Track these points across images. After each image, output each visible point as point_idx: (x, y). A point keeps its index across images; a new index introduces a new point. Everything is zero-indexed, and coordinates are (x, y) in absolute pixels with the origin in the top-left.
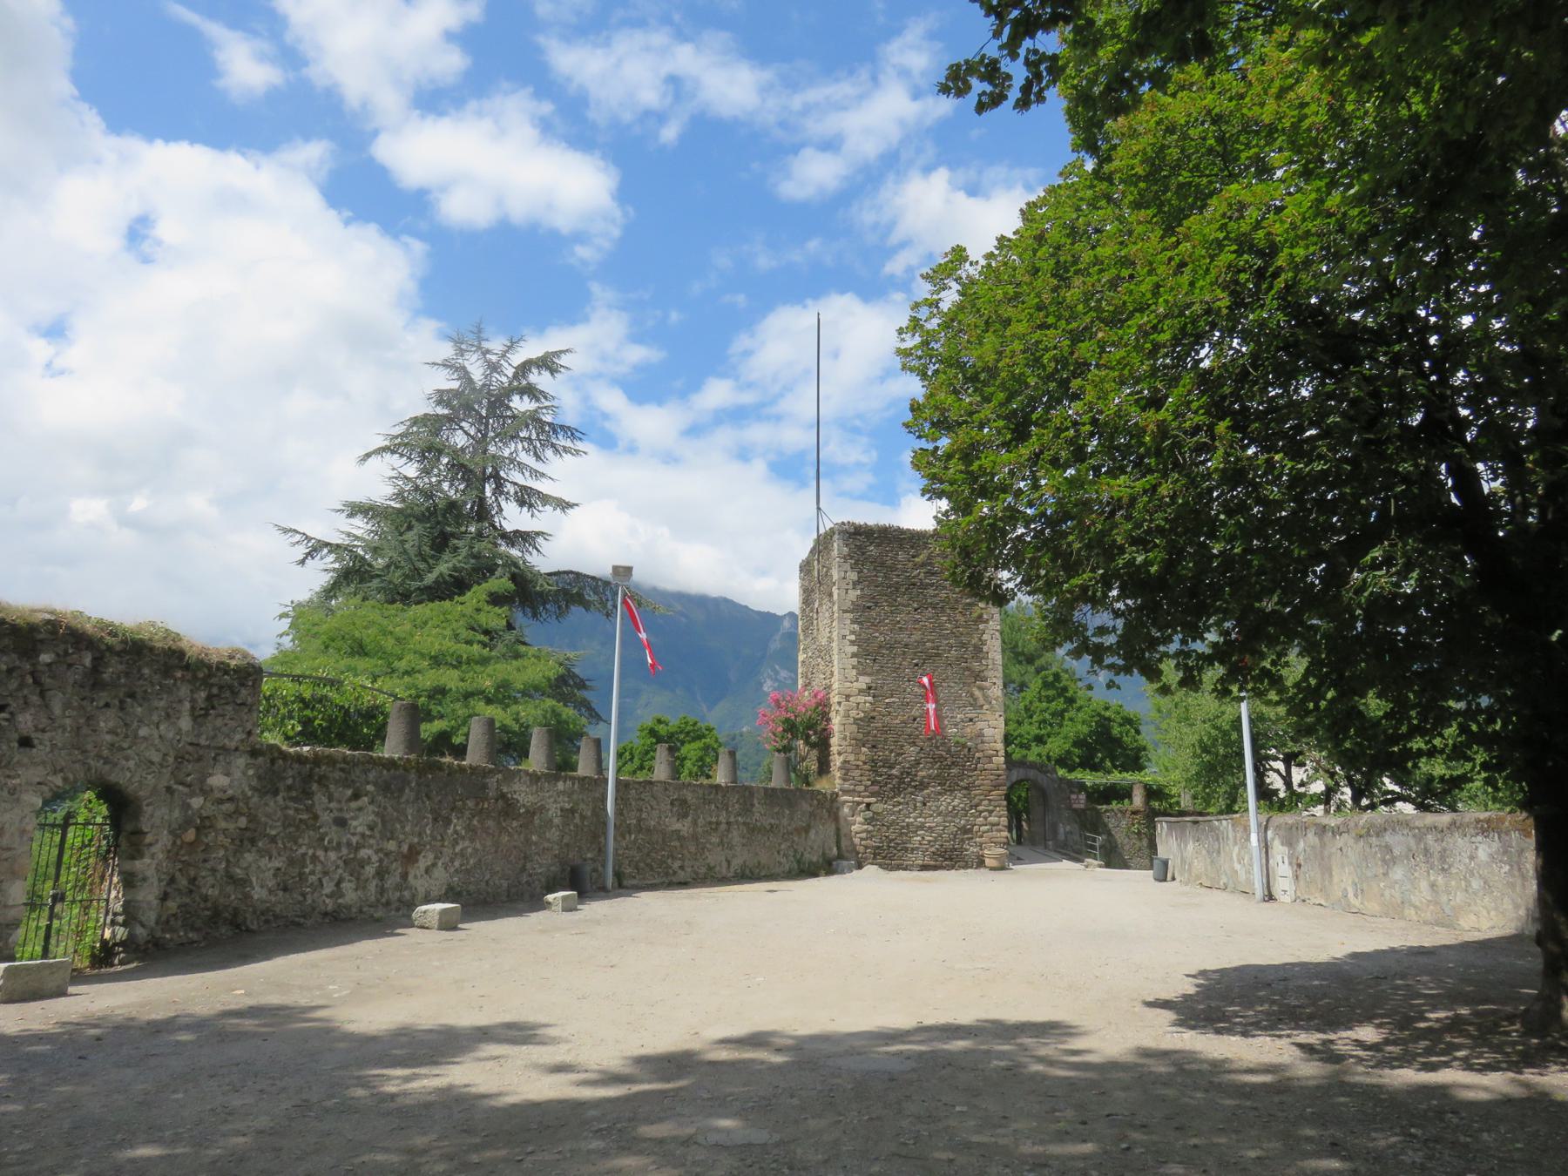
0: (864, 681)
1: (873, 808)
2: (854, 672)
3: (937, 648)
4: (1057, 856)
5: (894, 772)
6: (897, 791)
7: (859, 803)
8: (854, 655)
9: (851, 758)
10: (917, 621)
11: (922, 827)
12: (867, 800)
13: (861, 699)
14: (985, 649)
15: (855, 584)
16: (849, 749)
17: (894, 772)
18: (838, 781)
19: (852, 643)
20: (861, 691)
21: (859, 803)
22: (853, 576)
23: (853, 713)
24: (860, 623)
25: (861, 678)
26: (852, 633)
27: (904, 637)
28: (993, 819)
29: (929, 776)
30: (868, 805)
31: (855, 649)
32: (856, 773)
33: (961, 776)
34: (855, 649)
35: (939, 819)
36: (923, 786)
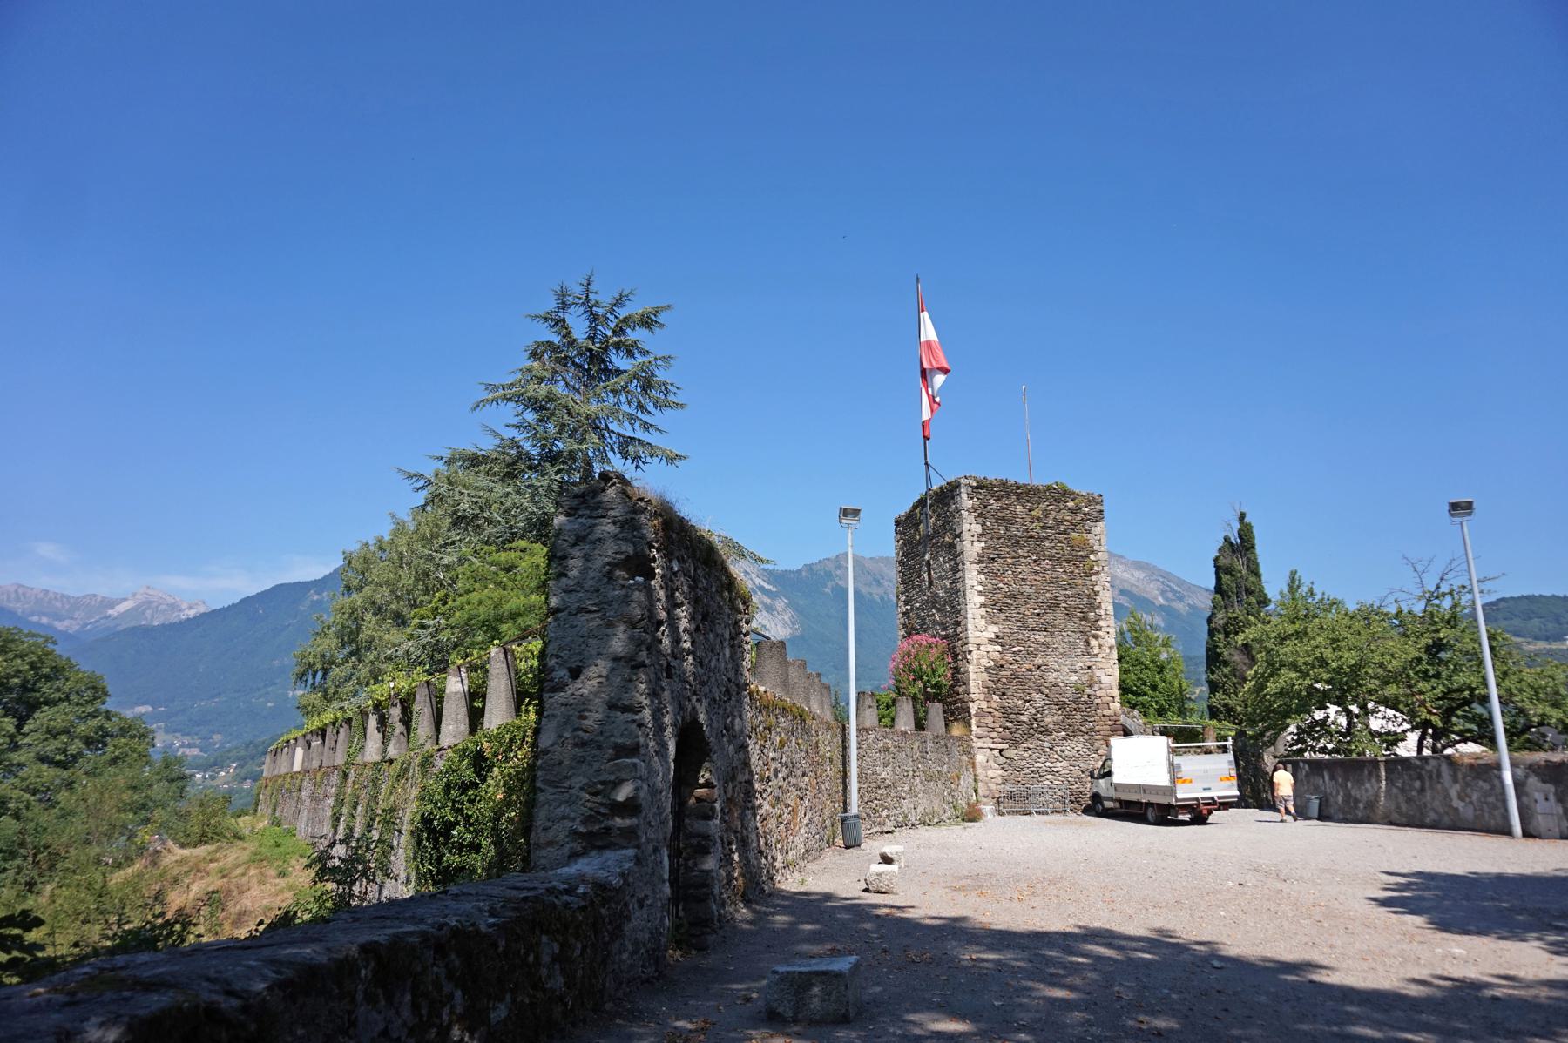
1: (1005, 753)
5: (1021, 718)
8: (983, 605)
9: (984, 705)
13: (991, 648)
17: (1021, 718)
23: (984, 662)
32: (989, 720)
35: (1065, 763)
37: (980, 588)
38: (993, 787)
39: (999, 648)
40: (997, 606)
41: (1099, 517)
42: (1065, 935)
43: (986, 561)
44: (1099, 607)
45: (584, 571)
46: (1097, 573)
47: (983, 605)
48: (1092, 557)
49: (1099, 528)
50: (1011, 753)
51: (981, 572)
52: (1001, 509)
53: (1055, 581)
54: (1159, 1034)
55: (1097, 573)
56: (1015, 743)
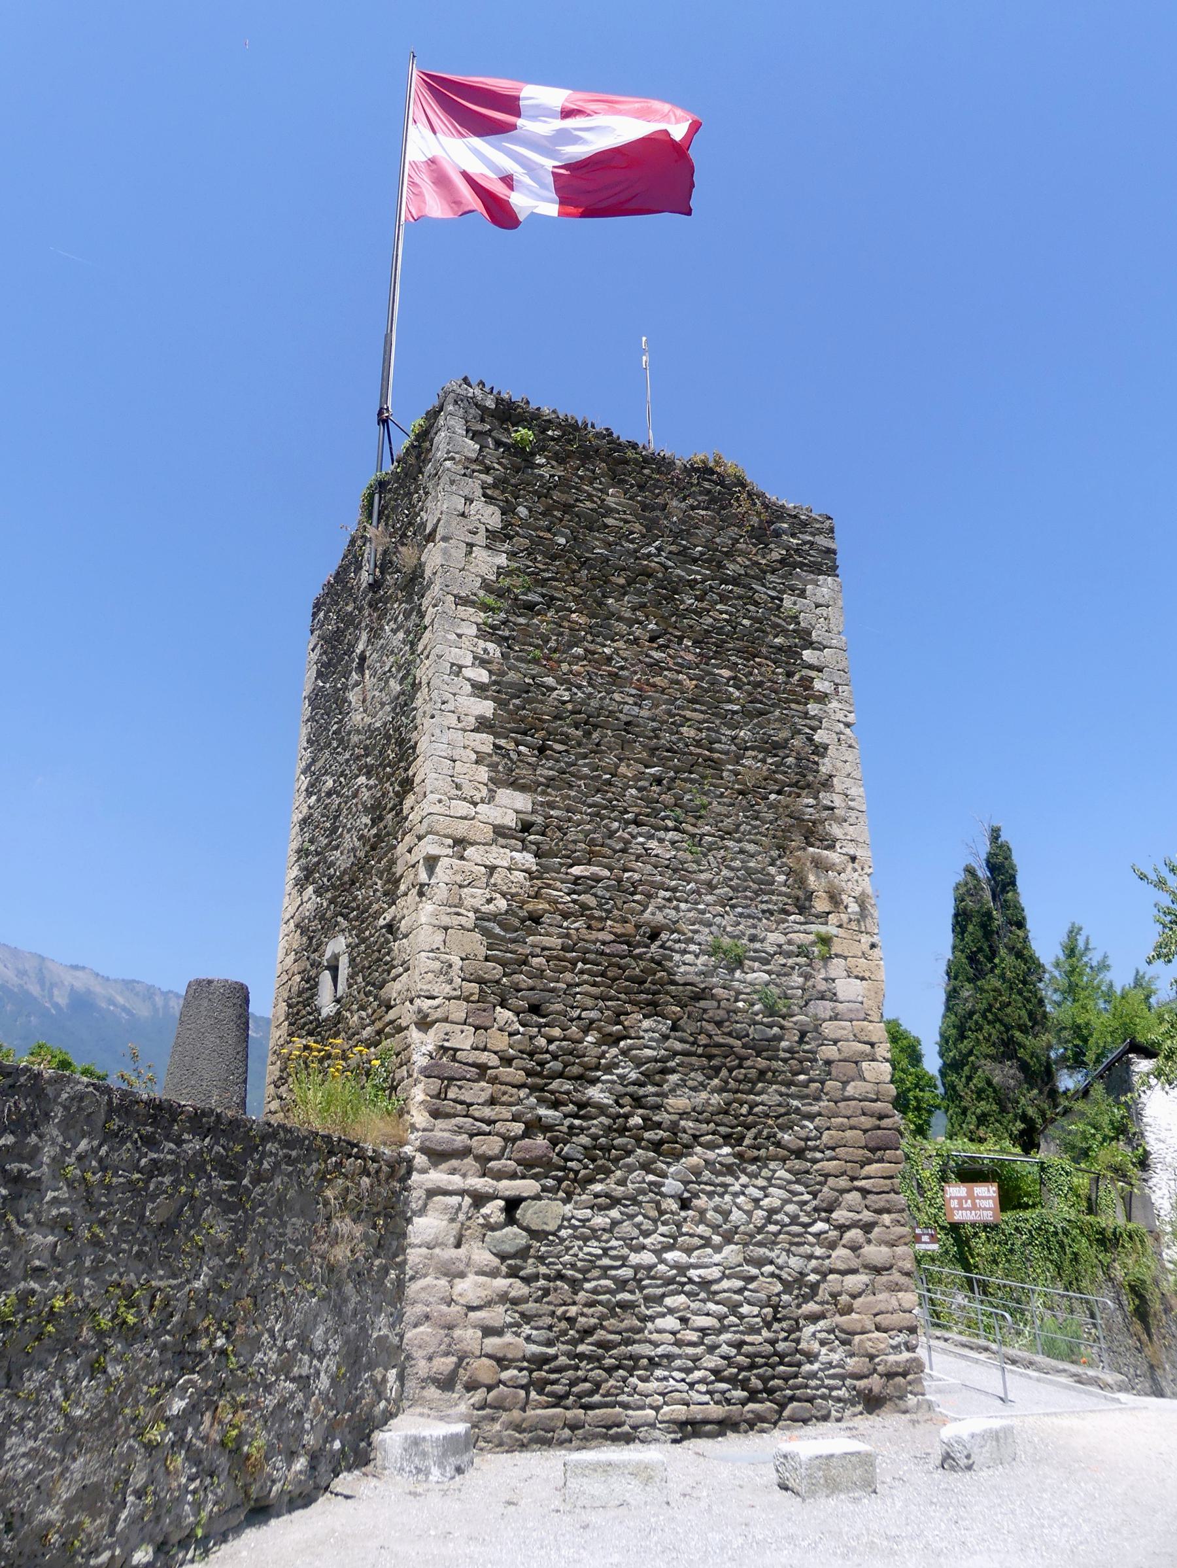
0: (511, 805)
1: (527, 1213)
2: (483, 773)
3: (710, 745)
4: (657, 136)
5: (595, 1093)
6: (603, 1157)
7: (480, 1200)
8: (483, 725)
9: (464, 1039)
10: (656, 667)
11: (677, 1281)
12: (510, 1187)
13: (500, 856)
14: (825, 767)
15: (495, 537)
16: (459, 1010)
17: (595, 1093)
18: (419, 1117)
19: (479, 689)
20: (500, 831)
21: (480, 1200)
22: (492, 517)
23: (475, 897)
24: (501, 640)
25: (506, 796)
26: (483, 662)
27: (623, 702)
28: (875, 1253)
29: (696, 1114)
30: (512, 1205)
31: (486, 708)
32: (479, 1092)
33: (786, 1118)
34: (486, 708)
35: (731, 1253)
36: (671, 1146)
37: (483, 676)
38: (469, 1337)
39: (528, 859)
40: (525, 730)
41: (825, 563)
42: (662, 464)
43: (509, 611)
44: (827, 784)
45: (255, 1412)
46: (823, 698)
47: (483, 725)
48: (807, 655)
49: (823, 588)
50: (548, 1212)
51: (488, 632)
52: (564, 484)
53: (709, 698)
54: (610, 1464)
55: (823, 698)
56: (564, 1179)
